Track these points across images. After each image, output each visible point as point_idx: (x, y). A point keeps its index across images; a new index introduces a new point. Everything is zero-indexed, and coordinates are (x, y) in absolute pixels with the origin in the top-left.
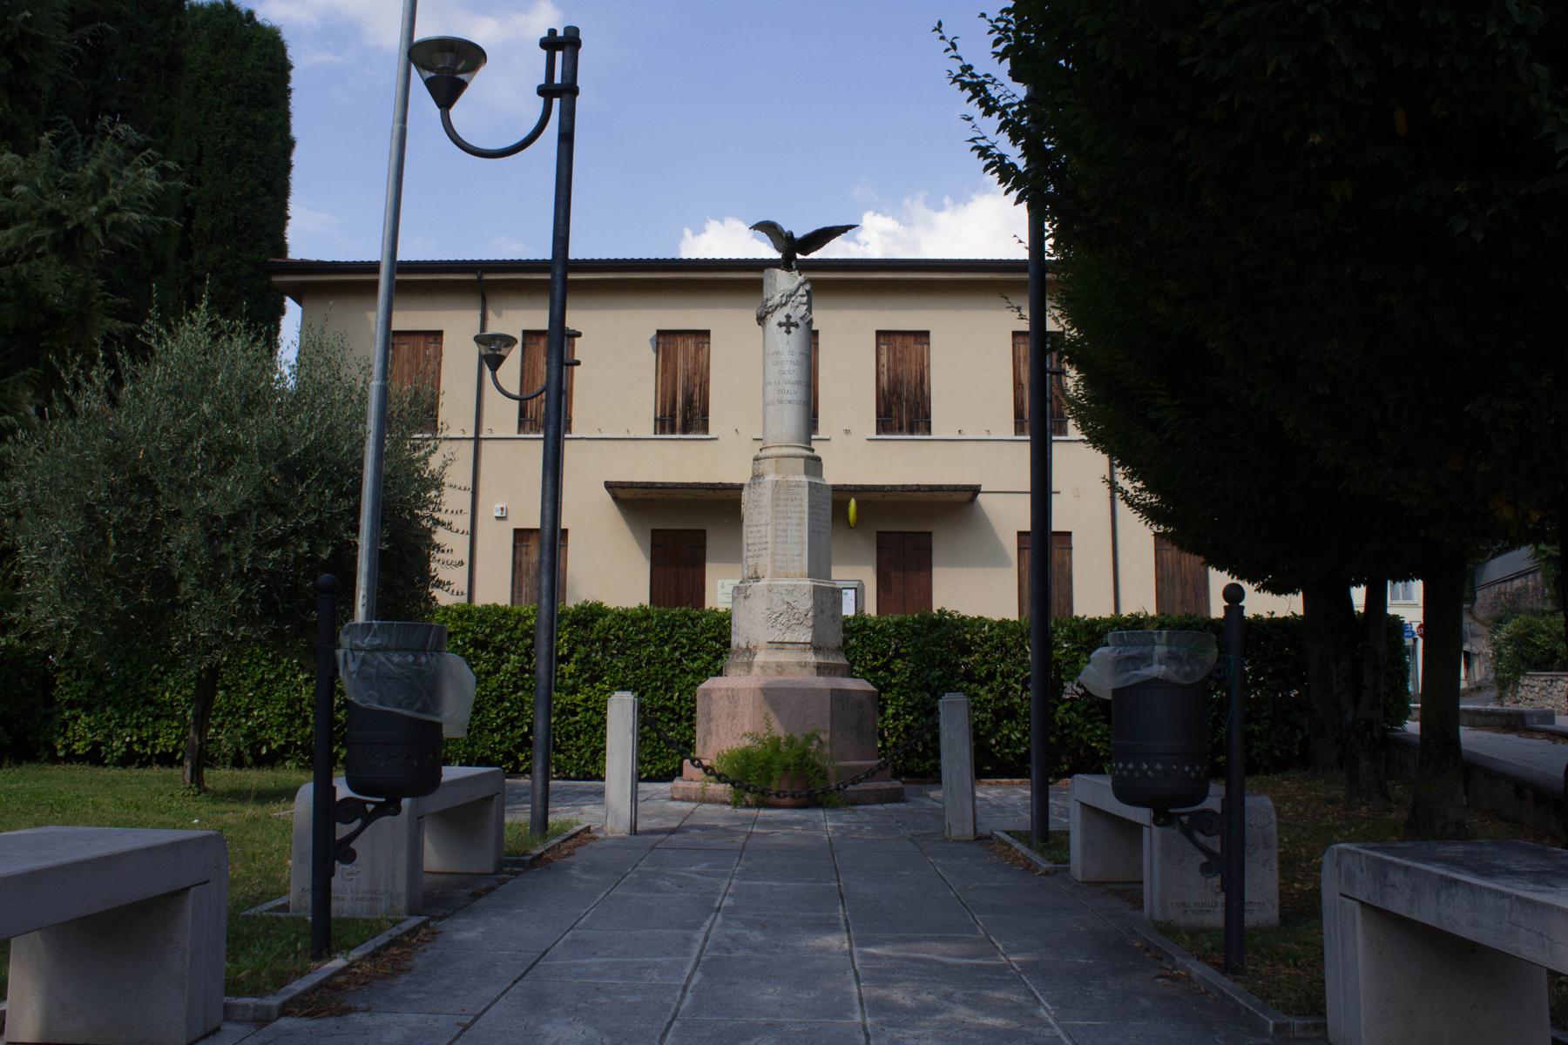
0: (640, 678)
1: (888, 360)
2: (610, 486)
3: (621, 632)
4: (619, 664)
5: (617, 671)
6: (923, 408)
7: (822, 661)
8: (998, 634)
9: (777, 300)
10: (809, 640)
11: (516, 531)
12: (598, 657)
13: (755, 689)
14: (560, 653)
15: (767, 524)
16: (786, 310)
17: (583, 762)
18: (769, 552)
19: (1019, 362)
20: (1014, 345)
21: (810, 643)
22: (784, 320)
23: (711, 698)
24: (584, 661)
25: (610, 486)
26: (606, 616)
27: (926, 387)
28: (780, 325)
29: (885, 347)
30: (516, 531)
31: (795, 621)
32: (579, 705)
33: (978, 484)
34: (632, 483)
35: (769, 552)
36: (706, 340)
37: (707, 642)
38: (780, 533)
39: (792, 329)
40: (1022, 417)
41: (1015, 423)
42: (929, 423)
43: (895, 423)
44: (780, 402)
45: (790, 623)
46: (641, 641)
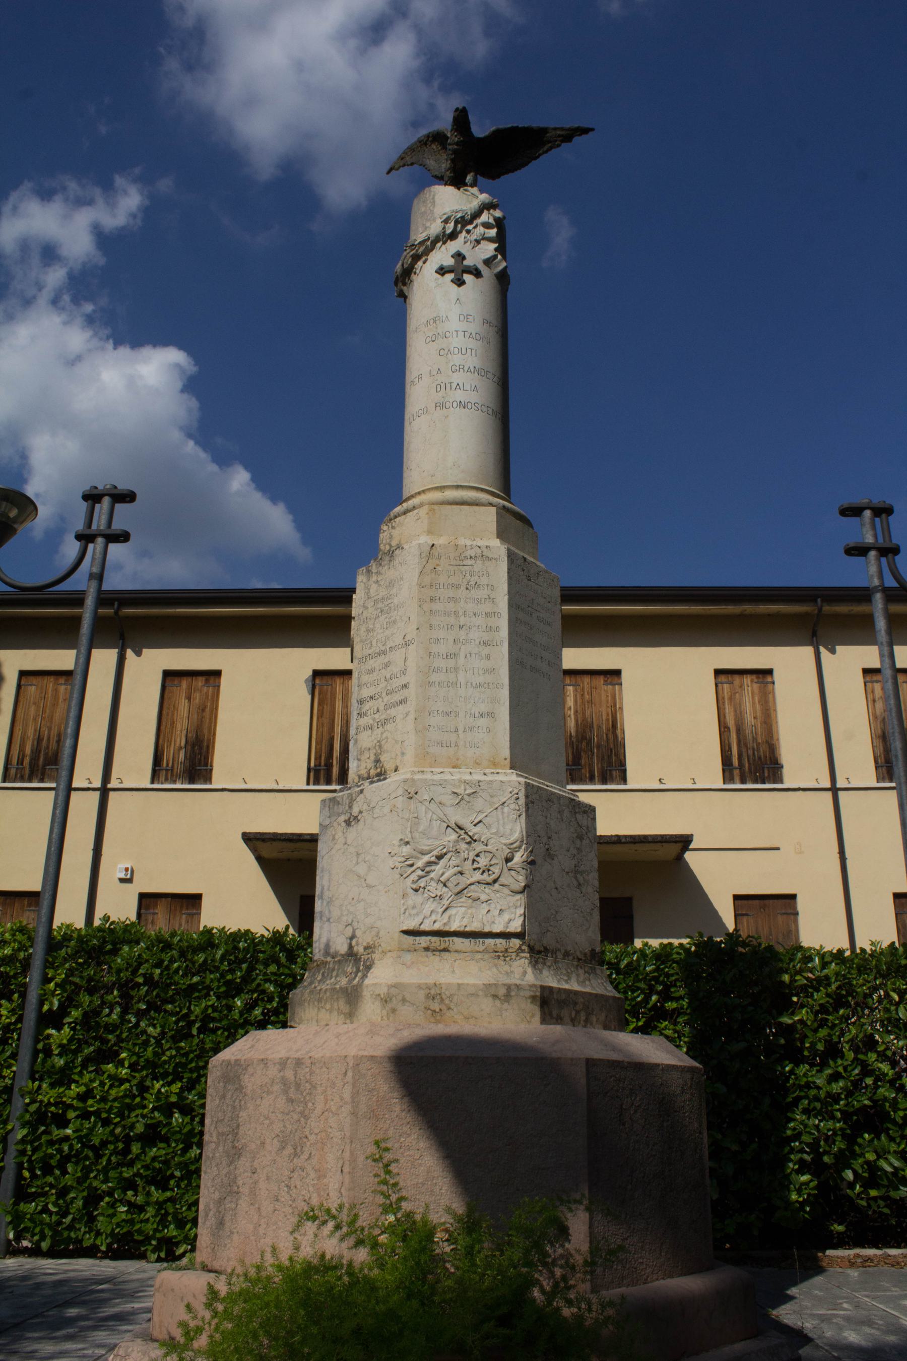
0: (186, 1055)
1: (576, 702)
2: (250, 839)
3: (158, 971)
4: (151, 1030)
5: (146, 1043)
6: (616, 755)
7: (554, 984)
8: (837, 974)
9: (435, 228)
10: (516, 926)
11: (143, 897)
12: (114, 1016)
13: (359, 1061)
14: (46, 1008)
16: (454, 246)
17: (68, 1220)
18: (411, 706)
19: (724, 703)
20: (716, 685)
21: (519, 935)
22: (450, 262)
23: (240, 1088)
24: (89, 1020)
25: (250, 839)
26: (138, 943)
27: (619, 732)
28: (442, 271)
29: (571, 688)
30: (143, 897)
31: (477, 876)
32: (71, 1106)
33: (689, 833)
34: (275, 834)
35: (411, 706)
38: (440, 663)
39: (467, 277)
40: (731, 764)
41: (724, 771)
42: (624, 772)
44: (440, 405)
45: (464, 881)
46: (192, 988)
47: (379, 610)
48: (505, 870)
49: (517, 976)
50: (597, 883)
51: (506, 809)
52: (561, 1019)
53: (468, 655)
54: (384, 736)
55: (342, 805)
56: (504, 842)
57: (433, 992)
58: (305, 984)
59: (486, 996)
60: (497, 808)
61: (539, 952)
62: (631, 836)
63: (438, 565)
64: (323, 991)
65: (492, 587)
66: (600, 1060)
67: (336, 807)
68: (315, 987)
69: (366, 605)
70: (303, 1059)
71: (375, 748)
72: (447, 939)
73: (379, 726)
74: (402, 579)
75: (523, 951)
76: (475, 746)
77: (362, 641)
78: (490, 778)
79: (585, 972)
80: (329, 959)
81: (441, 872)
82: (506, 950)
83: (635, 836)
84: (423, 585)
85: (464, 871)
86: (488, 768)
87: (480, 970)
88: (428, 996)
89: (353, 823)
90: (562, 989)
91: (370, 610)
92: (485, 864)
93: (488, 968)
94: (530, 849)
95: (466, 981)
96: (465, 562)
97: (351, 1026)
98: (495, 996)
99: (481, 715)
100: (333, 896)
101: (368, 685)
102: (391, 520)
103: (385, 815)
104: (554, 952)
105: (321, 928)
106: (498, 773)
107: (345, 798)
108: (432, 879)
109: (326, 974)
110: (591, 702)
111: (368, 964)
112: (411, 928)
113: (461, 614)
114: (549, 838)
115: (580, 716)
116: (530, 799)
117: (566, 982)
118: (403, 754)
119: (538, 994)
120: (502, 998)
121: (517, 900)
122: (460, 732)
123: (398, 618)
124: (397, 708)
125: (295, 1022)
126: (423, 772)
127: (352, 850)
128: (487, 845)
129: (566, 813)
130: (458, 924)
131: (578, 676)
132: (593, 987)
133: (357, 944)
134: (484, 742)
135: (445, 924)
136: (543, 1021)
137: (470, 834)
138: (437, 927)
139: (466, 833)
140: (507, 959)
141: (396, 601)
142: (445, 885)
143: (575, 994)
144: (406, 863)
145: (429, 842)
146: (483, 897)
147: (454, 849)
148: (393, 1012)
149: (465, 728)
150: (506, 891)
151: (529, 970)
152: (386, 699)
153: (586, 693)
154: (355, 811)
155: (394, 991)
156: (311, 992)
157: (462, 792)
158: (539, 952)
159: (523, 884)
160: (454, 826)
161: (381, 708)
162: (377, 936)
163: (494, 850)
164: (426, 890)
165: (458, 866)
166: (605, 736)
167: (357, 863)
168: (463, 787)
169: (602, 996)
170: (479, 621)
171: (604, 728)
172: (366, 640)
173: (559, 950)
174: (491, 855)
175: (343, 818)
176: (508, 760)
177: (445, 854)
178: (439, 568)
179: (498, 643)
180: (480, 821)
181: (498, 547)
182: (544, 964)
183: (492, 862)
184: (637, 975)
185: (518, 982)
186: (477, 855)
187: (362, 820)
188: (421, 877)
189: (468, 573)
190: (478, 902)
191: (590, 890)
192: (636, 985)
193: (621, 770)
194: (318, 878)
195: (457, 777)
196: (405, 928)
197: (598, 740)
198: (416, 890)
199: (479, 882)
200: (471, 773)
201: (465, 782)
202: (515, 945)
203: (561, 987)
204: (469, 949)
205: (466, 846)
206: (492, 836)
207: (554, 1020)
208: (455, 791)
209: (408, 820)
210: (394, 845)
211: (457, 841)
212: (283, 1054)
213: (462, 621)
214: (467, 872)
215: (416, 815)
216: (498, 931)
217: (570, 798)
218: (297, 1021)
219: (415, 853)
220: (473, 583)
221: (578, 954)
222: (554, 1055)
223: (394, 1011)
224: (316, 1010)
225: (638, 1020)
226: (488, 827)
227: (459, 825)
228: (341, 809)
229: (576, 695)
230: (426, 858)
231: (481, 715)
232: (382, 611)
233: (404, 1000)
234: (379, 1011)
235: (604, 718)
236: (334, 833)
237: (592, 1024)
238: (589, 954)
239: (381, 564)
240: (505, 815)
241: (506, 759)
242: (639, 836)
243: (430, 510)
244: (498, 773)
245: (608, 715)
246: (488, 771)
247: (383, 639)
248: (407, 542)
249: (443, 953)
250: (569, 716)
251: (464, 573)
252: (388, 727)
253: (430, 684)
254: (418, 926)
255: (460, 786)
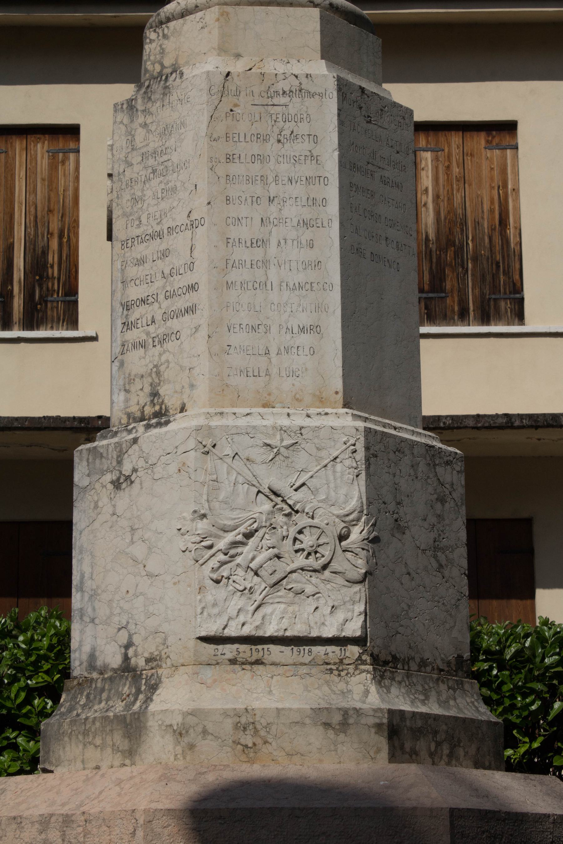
1: (436, 179)
6: (507, 273)
7: (407, 707)
15: (193, 226)
27: (511, 232)
29: (428, 155)
31: (300, 560)
36: (72, 145)
37: (28, 701)
43: (453, 303)
45: (283, 567)
47: (150, 170)
48: (339, 551)
49: (356, 697)
50: (464, 563)
51: (339, 467)
52: (417, 754)
53: (282, 242)
54: (163, 358)
55: (108, 459)
56: (336, 512)
57: (243, 720)
58: (63, 710)
59: (315, 724)
60: (326, 466)
61: (386, 663)
62: (530, 416)
63: (236, 105)
64: (91, 720)
65: (315, 139)
66: (469, 810)
67: (98, 461)
68: (78, 715)
69: (129, 159)
70: (73, 815)
71: (150, 375)
72: (260, 647)
73: (156, 343)
74: (183, 124)
75: (364, 663)
76: (293, 374)
77: (125, 215)
78: (315, 422)
79: (449, 688)
80: (95, 675)
81: (250, 556)
82: (341, 661)
83: (538, 415)
84: (215, 136)
85: (283, 554)
86: (312, 406)
87: (306, 688)
88: (236, 726)
89: (124, 486)
90: (417, 712)
91: (136, 168)
92: (311, 543)
93: (317, 686)
94: (373, 521)
95: (287, 705)
96: (276, 101)
97: (136, 770)
98: (327, 725)
99: (302, 330)
100: (98, 587)
101: (138, 282)
102: (161, 23)
103: (170, 476)
104: (406, 662)
105: (82, 632)
106: (326, 414)
107: (110, 450)
108: (238, 565)
109: (92, 697)
110: (463, 179)
111: (153, 682)
112: (212, 634)
113: (270, 179)
114: (399, 503)
115: (444, 206)
116: (372, 451)
117: (423, 702)
118: (192, 386)
119: (385, 721)
120: (337, 727)
121: (356, 593)
122: (273, 354)
123: (178, 184)
124: (181, 319)
125: (50, 763)
126: (221, 413)
127: (124, 523)
128: (313, 518)
129: (422, 467)
130: (276, 627)
131: (440, 133)
132: (460, 710)
133: (136, 655)
134: (306, 369)
135: (257, 627)
136: (393, 758)
137: (291, 502)
138: (246, 631)
139: (284, 501)
140: (343, 674)
141: (175, 158)
142: (256, 574)
143: (435, 719)
144: (203, 544)
145: (234, 514)
146: (309, 589)
147: (268, 524)
148: (190, 749)
149: (279, 349)
150: (340, 580)
151: (373, 689)
152: (165, 304)
153: (454, 164)
154: (127, 469)
155: (191, 720)
156: (73, 722)
157: (278, 444)
158: (386, 663)
159: (363, 571)
160: (267, 491)
161: (158, 318)
162: (164, 644)
163: (323, 525)
164: (231, 581)
165: (273, 547)
166: (487, 240)
167: (132, 542)
168: (278, 437)
169: (472, 720)
170: (297, 190)
171: (486, 225)
172: (131, 214)
173: (413, 658)
174: (319, 531)
175: (108, 477)
176: (341, 395)
177: (256, 531)
178: (237, 110)
179: (325, 224)
180: (303, 484)
181: (324, 76)
182: (393, 679)
183: (321, 541)
184: (531, 670)
185: (358, 705)
186: (300, 532)
187: (138, 481)
188: (223, 563)
189: (280, 116)
190: (302, 596)
191: (455, 572)
192: (528, 685)
193: (514, 299)
194: (74, 562)
195: (269, 422)
196: (203, 634)
197: (475, 247)
198: (217, 582)
199: (302, 569)
200: (288, 415)
201: (281, 429)
202: (353, 654)
203: (416, 710)
204: (291, 662)
205: (285, 519)
206: (320, 505)
207: (407, 756)
208: (268, 442)
209: (203, 484)
210: (184, 518)
211: (272, 512)
212: (44, 810)
213: (273, 190)
214: (286, 555)
215: (214, 477)
216: (330, 636)
217: (427, 445)
218: (54, 761)
219: (214, 530)
220: (287, 132)
221: (439, 662)
222: (408, 804)
223: (192, 747)
224: (81, 746)
225: (533, 739)
226: (314, 492)
227: (275, 490)
228: (106, 464)
229: (437, 168)
230: (230, 537)
231: (302, 330)
232: (154, 172)
233: (205, 732)
234: (170, 747)
235: (486, 207)
236: (96, 499)
237: (458, 759)
238: (453, 662)
239: (150, 98)
240: (338, 475)
241: (337, 393)
242: (544, 415)
243: (222, 15)
244: (326, 414)
245: (492, 202)
246: (312, 411)
247: (158, 215)
248: (187, 63)
249: (255, 667)
250: (425, 205)
251: (274, 117)
252: (169, 345)
253: (228, 285)
254: (220, 630)
255: (274, 435)
